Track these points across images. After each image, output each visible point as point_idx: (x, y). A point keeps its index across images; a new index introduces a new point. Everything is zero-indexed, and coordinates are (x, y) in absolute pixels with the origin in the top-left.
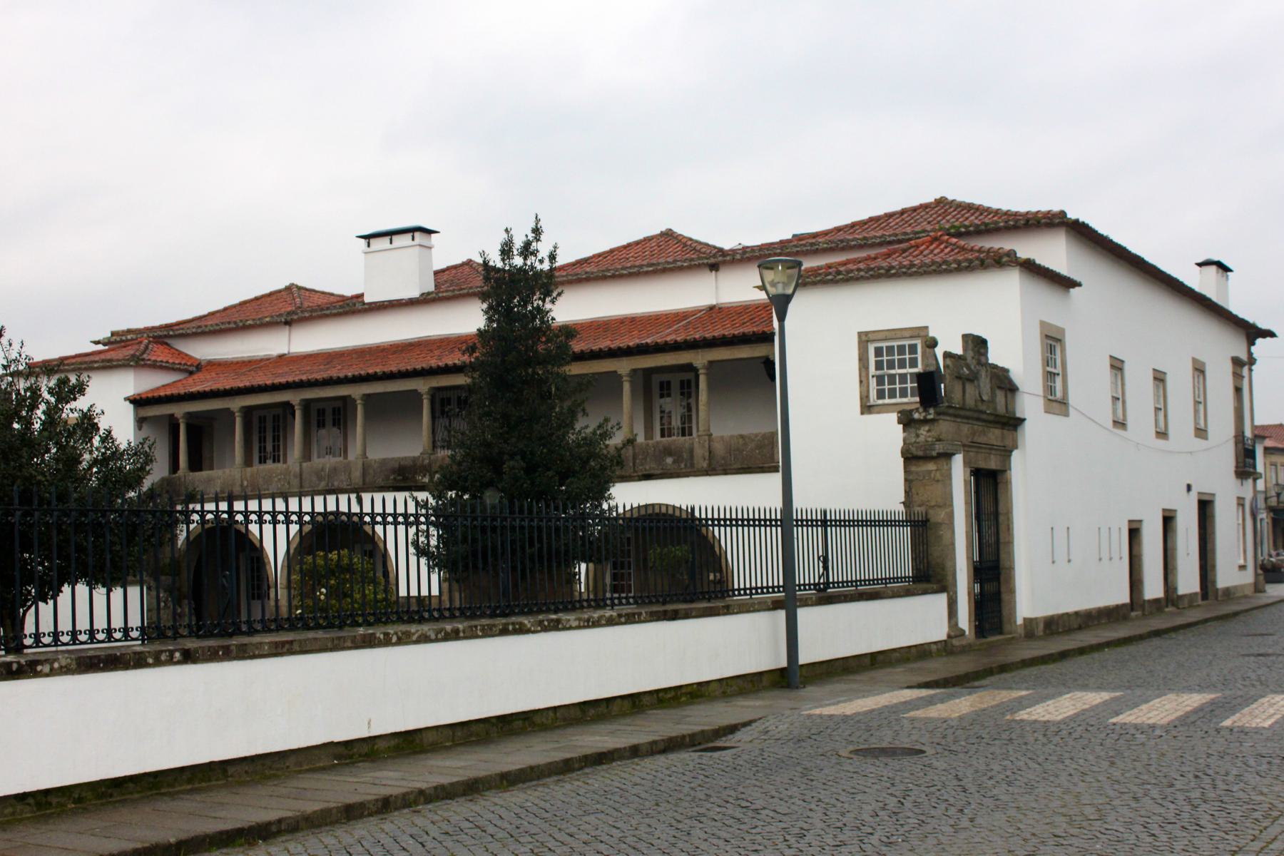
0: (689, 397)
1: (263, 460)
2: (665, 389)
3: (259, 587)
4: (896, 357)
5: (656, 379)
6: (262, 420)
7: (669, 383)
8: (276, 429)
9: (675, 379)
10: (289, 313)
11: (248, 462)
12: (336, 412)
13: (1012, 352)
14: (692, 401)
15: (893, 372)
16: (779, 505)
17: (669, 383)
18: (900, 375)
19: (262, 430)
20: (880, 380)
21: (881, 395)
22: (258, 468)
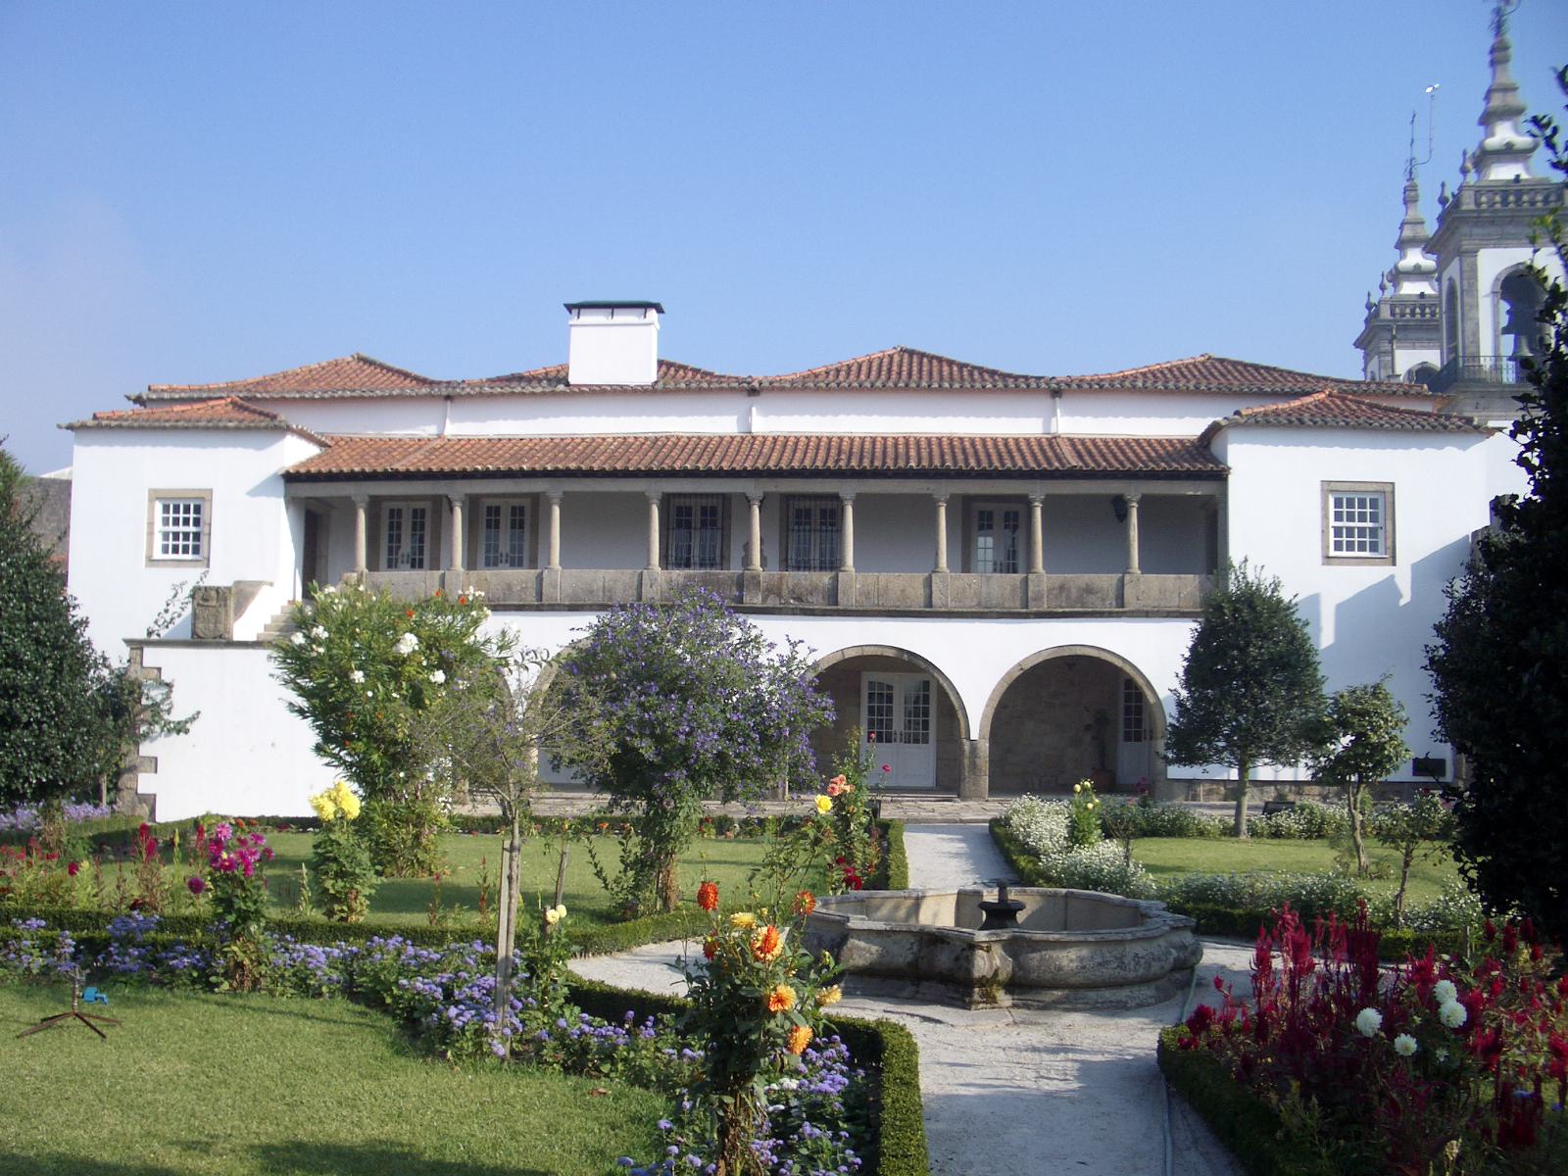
0: (1015, 528)
1: (392, 565)
2: (986, 523)
3: (1139, 723)
4: (1357, 510)
5: (387, 506)
6: (396, 514)
7: (400, 511)
8: (418, 527)
9: (999, 510)
10: (162, 390)
11: (373, 565)
12: (517, 512)
13: (693, 505)
14: (1021, 534)
15: (1351, 524)
16: (236, 638)
17: (400, 511)
18: (1347, 528)
19: (395, 527)
20: (1338, 532)
21: (1338, 546)
22: (385, 576)
